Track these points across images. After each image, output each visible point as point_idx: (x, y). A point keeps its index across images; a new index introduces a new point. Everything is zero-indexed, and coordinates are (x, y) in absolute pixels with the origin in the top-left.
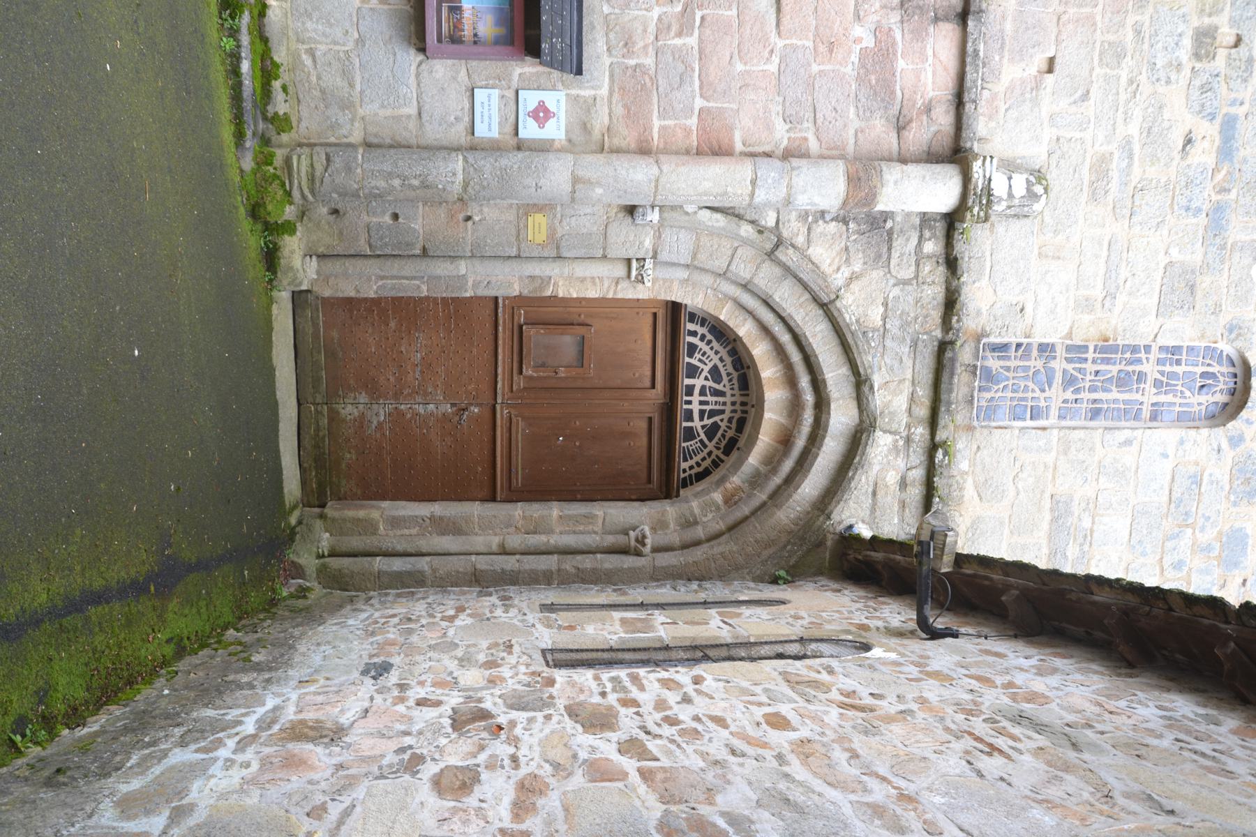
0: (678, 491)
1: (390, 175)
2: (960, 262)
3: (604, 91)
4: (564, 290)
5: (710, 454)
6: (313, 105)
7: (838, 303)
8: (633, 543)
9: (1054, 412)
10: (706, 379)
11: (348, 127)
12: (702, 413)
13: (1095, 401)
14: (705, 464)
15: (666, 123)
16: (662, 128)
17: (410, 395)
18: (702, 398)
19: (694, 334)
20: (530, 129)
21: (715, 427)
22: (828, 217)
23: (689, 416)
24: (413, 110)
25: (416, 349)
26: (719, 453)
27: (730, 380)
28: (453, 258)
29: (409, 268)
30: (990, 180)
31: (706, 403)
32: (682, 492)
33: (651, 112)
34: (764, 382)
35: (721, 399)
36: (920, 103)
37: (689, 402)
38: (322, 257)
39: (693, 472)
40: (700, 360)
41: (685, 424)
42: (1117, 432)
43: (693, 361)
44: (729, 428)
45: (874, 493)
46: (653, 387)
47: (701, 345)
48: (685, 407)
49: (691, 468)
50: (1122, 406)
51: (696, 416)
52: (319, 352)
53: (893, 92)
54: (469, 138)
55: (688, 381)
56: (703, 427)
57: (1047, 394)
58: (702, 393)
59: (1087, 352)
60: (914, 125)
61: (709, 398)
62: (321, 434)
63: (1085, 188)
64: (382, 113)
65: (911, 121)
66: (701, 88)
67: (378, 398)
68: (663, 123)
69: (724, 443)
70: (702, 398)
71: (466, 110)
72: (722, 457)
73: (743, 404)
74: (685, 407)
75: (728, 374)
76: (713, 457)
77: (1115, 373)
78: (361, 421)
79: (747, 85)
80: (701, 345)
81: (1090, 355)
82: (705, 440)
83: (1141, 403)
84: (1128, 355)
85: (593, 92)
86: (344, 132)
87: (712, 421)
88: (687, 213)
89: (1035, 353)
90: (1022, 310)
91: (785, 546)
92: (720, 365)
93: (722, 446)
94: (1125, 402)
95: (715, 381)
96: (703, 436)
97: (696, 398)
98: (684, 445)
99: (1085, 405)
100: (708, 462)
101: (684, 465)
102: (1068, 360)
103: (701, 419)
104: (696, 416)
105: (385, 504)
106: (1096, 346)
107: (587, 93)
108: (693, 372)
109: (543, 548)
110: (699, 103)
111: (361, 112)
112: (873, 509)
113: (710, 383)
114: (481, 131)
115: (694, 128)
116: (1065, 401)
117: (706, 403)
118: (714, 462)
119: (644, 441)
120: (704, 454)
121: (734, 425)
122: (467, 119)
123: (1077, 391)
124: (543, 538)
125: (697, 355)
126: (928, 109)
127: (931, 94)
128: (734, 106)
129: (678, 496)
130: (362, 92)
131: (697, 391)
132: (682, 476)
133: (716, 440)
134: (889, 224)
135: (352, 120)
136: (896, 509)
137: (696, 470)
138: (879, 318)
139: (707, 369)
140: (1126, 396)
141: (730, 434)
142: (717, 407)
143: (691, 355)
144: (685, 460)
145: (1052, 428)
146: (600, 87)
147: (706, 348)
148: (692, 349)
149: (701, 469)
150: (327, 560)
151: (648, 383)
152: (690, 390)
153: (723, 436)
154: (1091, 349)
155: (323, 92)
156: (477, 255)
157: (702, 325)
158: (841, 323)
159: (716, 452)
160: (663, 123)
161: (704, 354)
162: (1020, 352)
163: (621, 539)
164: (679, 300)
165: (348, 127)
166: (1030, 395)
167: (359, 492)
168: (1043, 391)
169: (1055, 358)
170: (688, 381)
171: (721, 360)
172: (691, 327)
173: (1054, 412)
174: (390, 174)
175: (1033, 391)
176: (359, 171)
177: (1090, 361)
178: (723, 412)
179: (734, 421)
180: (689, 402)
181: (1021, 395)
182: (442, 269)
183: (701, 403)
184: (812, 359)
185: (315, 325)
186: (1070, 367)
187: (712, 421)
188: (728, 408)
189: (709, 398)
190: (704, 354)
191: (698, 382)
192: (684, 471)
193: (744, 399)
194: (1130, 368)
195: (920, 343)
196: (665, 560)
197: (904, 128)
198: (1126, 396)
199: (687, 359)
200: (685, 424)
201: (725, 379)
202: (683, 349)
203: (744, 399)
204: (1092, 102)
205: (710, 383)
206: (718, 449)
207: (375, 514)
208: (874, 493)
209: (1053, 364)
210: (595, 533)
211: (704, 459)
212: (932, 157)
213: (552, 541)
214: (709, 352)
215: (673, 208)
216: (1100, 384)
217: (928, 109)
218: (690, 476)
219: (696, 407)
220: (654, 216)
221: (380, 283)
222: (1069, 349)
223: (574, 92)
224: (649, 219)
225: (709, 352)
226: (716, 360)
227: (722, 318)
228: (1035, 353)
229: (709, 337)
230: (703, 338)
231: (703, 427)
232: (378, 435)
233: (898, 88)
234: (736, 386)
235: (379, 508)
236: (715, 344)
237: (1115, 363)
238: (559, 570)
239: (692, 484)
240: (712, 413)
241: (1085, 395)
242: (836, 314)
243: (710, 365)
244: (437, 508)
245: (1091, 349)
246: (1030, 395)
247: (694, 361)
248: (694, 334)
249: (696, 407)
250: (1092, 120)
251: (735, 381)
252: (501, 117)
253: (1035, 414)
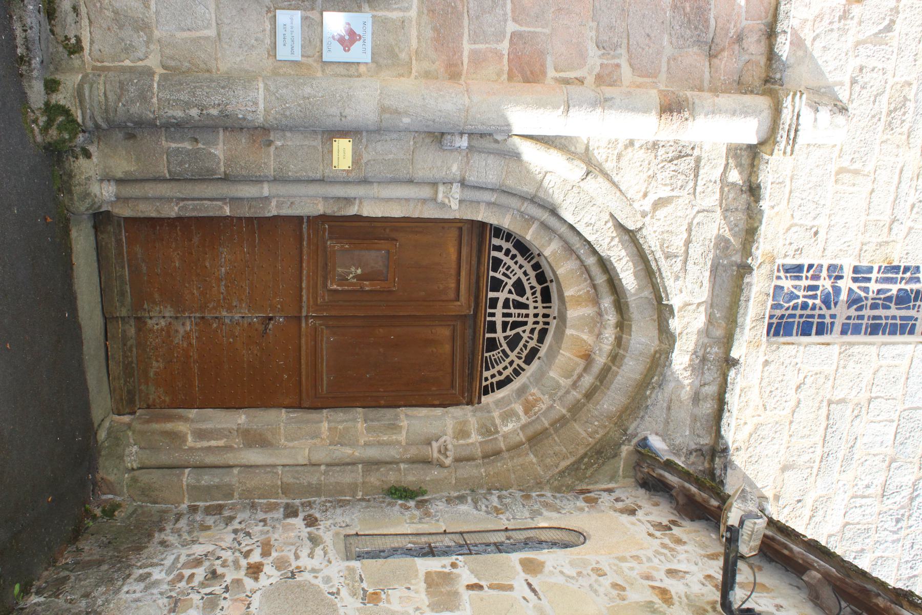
0: (480, 398)
1: (188, 105)
2: (762, 191)
3: (413, 13)
4: (370, 210)
5: (511, 363)
6: (105, 26)
7: (644, 231)
8: (436, 455)
9: (838, 328)
10: (510, 292)
11: (144, 49)
12: (505, 325)
13: (875, 318)
14: (506, 373)
15: (477, 46)
16: (473, 53)
17: (215, 308)
18: (506, 311)
19: (498, 248)
20: (334, 53)
21: (518, 337)
22: (637, 145)
23: (492, 327)
24: (212, 32)
25: (225, 261)
26: (521, 362)
27: (533, 294)
28: (258, 181)
29: (209, 190)
30: (798, 115)
31: (510, 315)
32: (483, 398)
33: (461, 36)
34: (566, 299)
35: (524, 312)
36: (732, 32)
37: (493, 315)
38: (120, 181)
39: (494, 380)
40: (504, 274)
41: (488, 335)
42: (892, 347)
43: (497, 275)
44: (532, 339)
45: (669, 408)
46: (457, 298)
47: (507, 260)
48: (488, 319)
49: (493, 376)
50: (898, 322)
51: (499, 327)
52: (123, 267)
53: (707, 21)
54: (271, 61)
55: (491, 295)
56: (505, 338)
57: (833, 311)
58: (506, 305)
59: (871, 272)
60: (726, 54)
61: (512, 310)
62: (129, 343)
63: (883, 118)
64: (180, 35)
65: (723, 50)
66: (513, 11)
67: (183, 311)
68: (473, 47)
69: (525, 352)
70: (506, 311)
71: (268, 32)
72: (523, 366)
73: (546, 316)
74: (488, 319)
75: (532, 288)
76: (515, 365)
77: (894, 292)
78: (169, 332)
79: (560, 9)
80: (507, 260)
81: (874, 275)
82: (508, 350)
83: (916, 319)
84: (908, 275)
85: (401, 14)
86: (140, 54)
87: (514, 332)
88: (496, 141)
89: (824, 273)
90: (816, 233)
91: (582, 458)
92: (524, 279)
93: (523, 356)
94: (902, 318)
95: (517, 294)
96: (505, 347)
97: (499, 310)
98: (486, 355)
99: (865, 321)
100: (510, 370)
101: (486, 374)
102: (855, 280)
103: (504, 330)
104: (499, 327)
105: (193, 413)
106: (880, 267)
107: (395, 15)
108: (497, 285)
109: (348, 460)
110: (511, 27)
111: (157, 34)
112: (667, 423)
113: (514, 296)
114: (283, 53)
115: (506, 52)
116: (849, 318)
117: (510, 315)
118: (515, 370)
119: (447, 348)
120: (506, 363)
121: (536, 336)
122: (268, 41)
123: (860, 309)
124: (348, 451)
125: (502, 270)
126: (739, 39)
127: (744, 23)
128: (547, 31)
129: (479, 402)
130: (157, 13)
131: (500, 304)
132: (484, 384)
133: (518, 349)
134: (696, 153)
135: (148, 43)
136: (688, 422)
137: (498, 378)
138: (682, 243)
139: (510, 282)
140: (904, 313)
141: (532, 344)
142: (520, 319)
143: (495, 270)
144: (487, 369)
145: (835, 343)
146: (407, 9)
147: (510, 263)
148: (497, 263)
149: (502, 377)
150: (136, 473)
151: (452, 295)
152: (494, 303)
153: (525, 346)
154: (876, 269)
155: (116, 12)
156: (280, 179)
157: (507, 240)
158: (645, 247)
159: (517, 361)
160: (473, 47)
161: (509, 268)
162: (811, 272)
163: (425, 451)
164: (484, 221)
165: (144, 49)
166: (817, 312)
167: (167, 399)
168: (829, 308)
169: (841, 277)
170: (491, 295)
171: (525, 274)
172: (496, 242)
173: (838, 328)
174: (187, 103)
175: (820, 309)
176: (155, 100)
177: (873, 281)
178: (525, 323)
179: (536, 332)
180: (493, 315)
181: (808, 312)
182: (247, 191)
183: (505, 315)
184: (616, 282)
185: (118, 242)
186: (855, 286)
187: (514, 332)
188: (531, 320)
189: (512, 310)
190: (509, 268)
191: (502, 296)
192: (486, 379)
193: (546, 311)
194: (908, 287)
195: (720, 268)
196: (467, 471)
197: (716, 56)
198: (904, 313)
199: (492, 274)
200: (488, 335)
201: (529, 292)
202: (487, 263)
203: (546, 311)
204: (896, 33)
205: (514, 296)
206: (520, 358)
207: (181, 427)
208: (669, 408)
209: (840, 283)
210: (399, 443)
211: (505, 368)
212: (741, 86)
213: (357, 454)
214: (514, 267)
215: (482, 135)
216: (880, 302)
217: (739, 39)
218: (492, 384)
219: (499, 320)
220: (464, 142)
221: (181, 204)
222: (856, 270)
223: (380, 14)
224: (457, 145)
225: (514, 267)
226: (520, 273)
227: (528, 237)
228: (824, 273)
229: (514, 251)
230: (507, 252)
231: (505, 338)
232: (185, 345)
233: (712, 16)
234: (539, 299)
235: (186, 420)
236: (519, 258)
237: (896, 283)
238: (363, 483)
239: (493, 391)
240: (515, 325)
241: (867, 312)
242: (641, 241)
243: (514, 279)
244: (241, 418)
245: (876, 269)
246: (817, 312)
247: (498, 275)
248: (498, 248)
249: (499, 320)
250: (896, 51)
251: (538, 294)
252: (303, 39)
253: (821, 330)
